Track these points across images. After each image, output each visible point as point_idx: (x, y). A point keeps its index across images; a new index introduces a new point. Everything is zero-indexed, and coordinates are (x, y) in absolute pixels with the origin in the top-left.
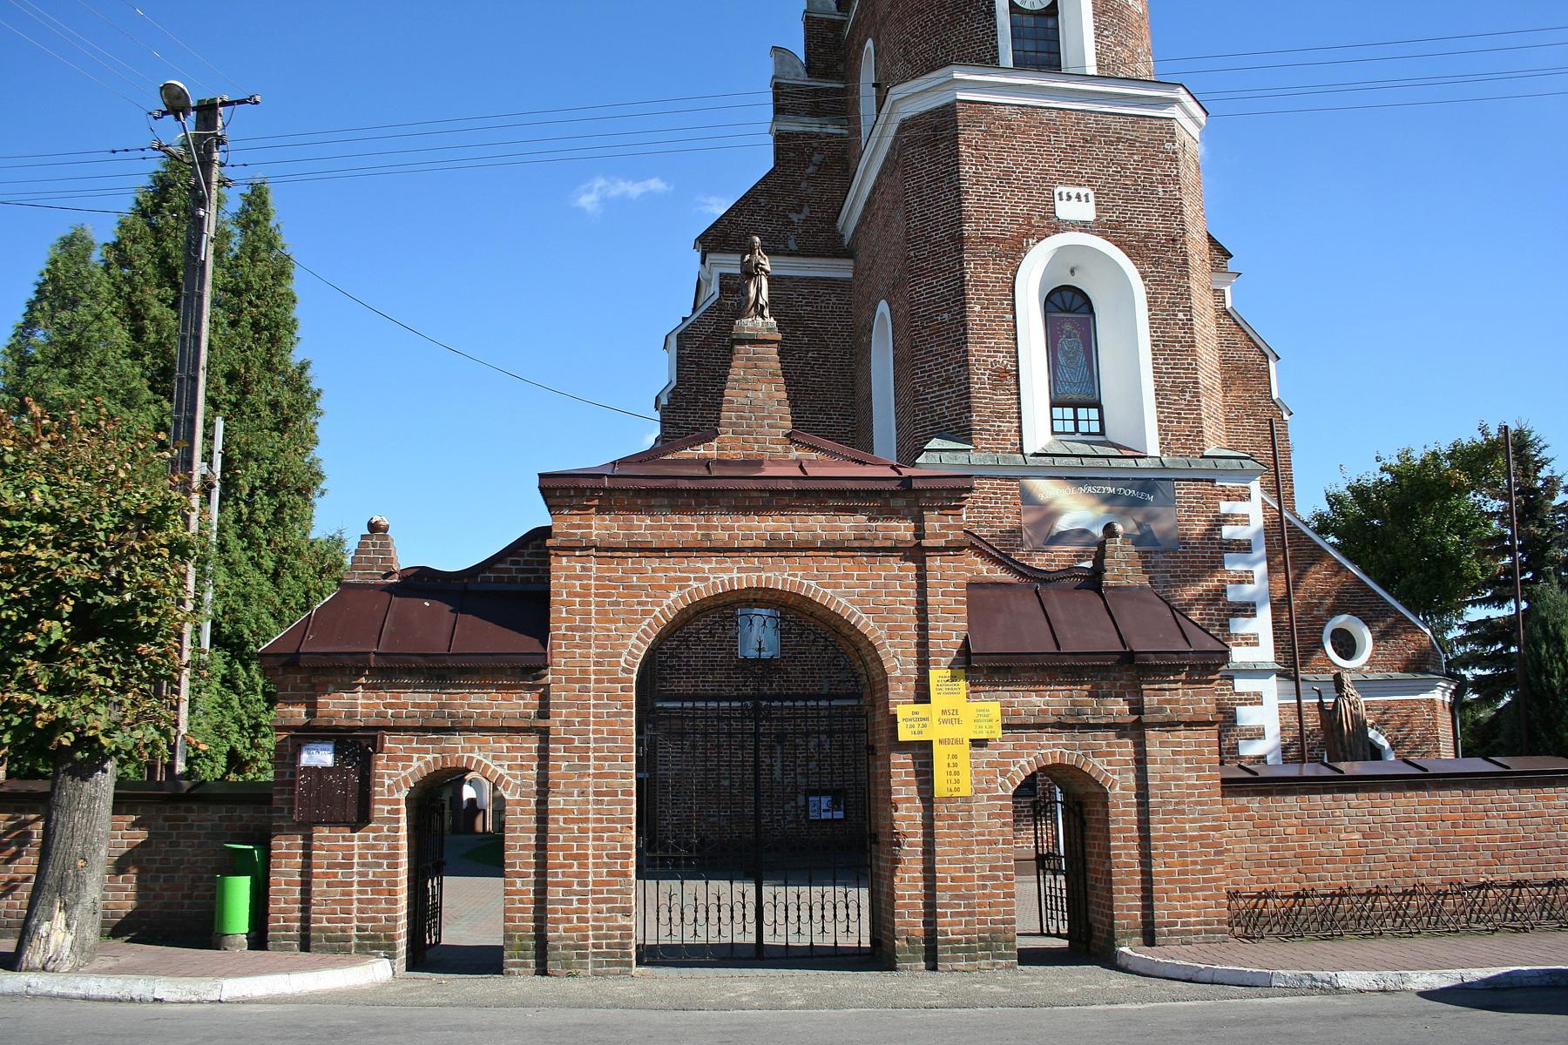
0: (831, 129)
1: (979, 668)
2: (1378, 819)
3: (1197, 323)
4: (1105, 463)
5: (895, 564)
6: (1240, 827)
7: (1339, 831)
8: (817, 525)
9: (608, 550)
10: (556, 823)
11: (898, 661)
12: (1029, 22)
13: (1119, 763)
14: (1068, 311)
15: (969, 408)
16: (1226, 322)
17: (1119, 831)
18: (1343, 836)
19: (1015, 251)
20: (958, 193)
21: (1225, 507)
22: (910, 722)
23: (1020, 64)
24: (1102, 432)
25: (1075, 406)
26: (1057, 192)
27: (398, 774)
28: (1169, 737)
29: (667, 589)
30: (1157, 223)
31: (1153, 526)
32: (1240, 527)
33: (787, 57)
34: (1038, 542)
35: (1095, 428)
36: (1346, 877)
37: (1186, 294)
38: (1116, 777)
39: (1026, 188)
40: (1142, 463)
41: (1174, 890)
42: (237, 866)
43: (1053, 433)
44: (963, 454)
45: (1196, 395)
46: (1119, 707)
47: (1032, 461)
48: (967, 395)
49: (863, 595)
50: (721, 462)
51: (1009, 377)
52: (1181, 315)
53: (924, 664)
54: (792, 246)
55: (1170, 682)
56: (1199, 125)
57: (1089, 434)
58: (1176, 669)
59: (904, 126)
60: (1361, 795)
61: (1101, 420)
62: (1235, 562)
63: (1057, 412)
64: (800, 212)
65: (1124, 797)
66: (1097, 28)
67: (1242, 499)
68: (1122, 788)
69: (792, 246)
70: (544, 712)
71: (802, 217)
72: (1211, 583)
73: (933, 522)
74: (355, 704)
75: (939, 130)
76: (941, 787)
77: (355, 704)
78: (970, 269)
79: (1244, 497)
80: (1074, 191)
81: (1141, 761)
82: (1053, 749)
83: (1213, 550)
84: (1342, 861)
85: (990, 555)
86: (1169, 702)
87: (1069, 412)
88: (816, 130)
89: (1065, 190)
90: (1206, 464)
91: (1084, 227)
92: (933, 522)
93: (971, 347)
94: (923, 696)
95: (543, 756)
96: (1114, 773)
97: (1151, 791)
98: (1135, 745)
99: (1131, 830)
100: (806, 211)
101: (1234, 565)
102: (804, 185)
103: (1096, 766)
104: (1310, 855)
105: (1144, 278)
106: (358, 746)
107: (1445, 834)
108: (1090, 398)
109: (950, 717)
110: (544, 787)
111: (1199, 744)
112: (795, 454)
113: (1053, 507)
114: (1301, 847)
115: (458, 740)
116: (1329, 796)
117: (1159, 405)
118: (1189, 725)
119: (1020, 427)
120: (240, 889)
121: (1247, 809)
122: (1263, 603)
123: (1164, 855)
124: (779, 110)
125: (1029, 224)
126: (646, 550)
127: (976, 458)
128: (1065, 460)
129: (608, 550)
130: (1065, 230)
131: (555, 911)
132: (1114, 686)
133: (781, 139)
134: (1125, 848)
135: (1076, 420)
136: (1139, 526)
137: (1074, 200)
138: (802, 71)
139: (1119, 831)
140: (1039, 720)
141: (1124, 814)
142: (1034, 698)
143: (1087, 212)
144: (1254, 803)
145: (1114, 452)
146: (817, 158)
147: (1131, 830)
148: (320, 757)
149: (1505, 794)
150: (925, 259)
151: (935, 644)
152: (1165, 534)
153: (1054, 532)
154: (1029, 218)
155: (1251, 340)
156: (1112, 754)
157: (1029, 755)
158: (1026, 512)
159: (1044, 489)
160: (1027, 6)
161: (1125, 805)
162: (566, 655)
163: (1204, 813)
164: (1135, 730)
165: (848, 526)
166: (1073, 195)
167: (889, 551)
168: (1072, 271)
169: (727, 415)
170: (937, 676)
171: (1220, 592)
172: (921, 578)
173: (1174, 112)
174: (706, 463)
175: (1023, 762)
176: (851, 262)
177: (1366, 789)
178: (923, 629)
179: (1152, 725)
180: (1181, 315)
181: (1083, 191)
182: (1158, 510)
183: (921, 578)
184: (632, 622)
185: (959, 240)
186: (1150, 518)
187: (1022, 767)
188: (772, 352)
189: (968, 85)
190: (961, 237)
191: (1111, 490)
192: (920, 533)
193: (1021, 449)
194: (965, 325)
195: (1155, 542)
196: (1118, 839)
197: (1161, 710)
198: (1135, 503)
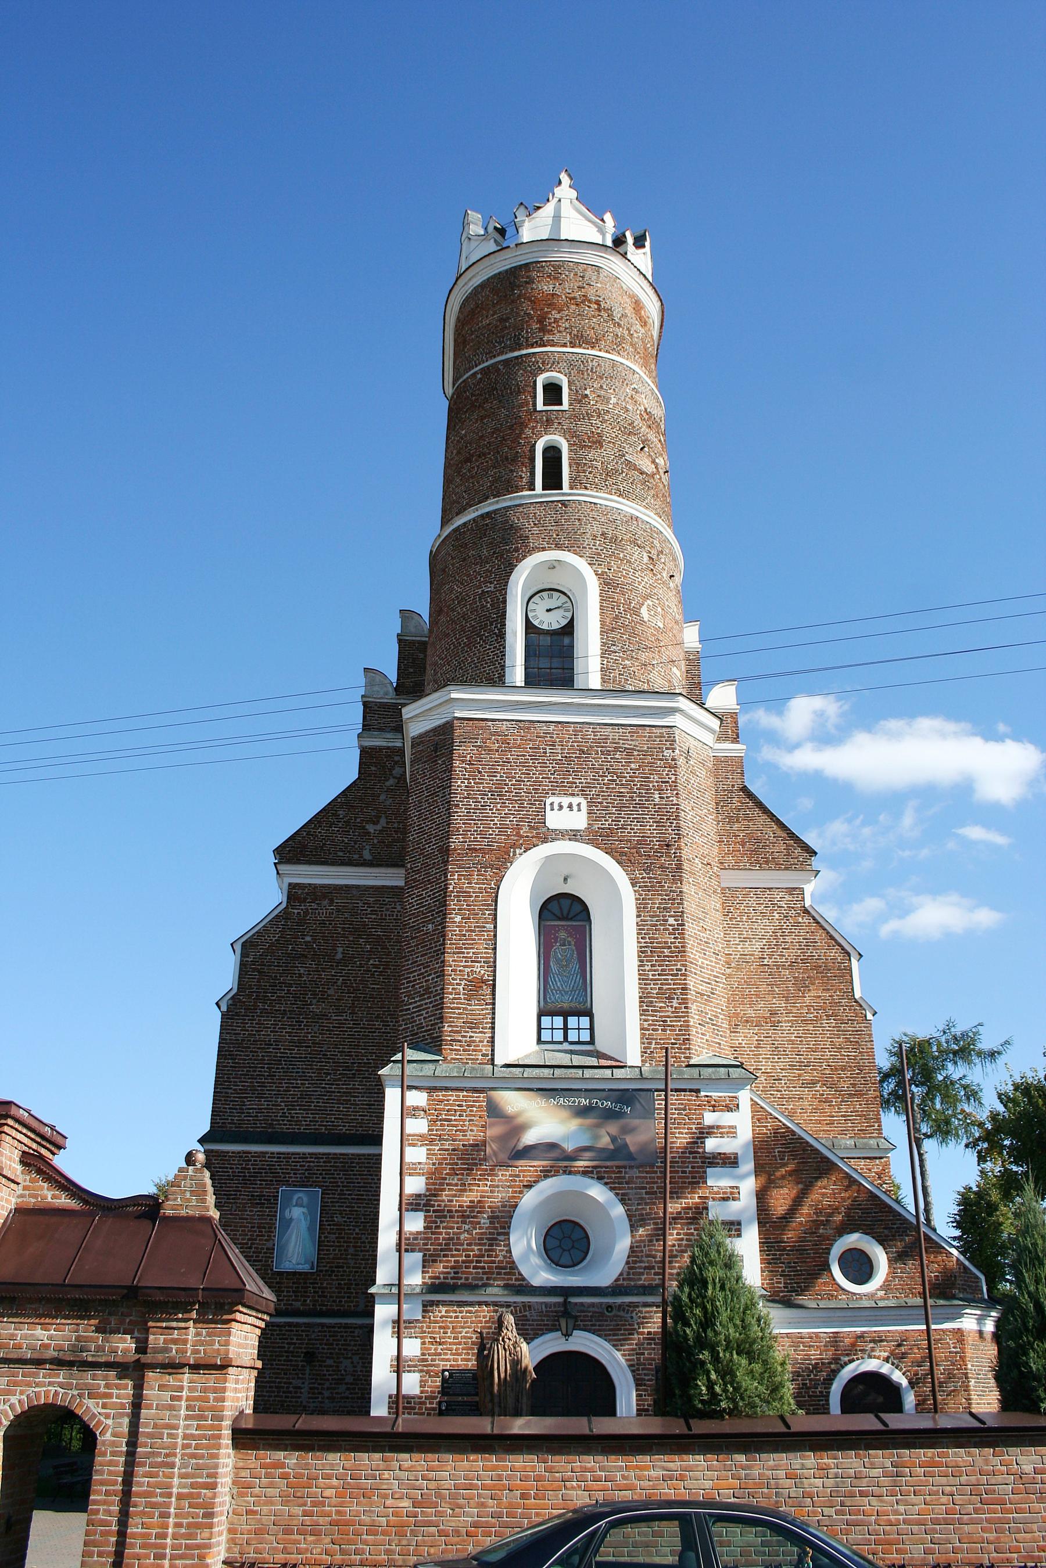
2: (433, 1485)
6: (271, 1486)
7: (386, 1497)
12: (547, 640)
13: (114, 1406)
14: (566, 919)
15: (441, 1018)
16: (804, 920)
17: (103, 1483)
18: (389, 1502)
19: (501, 862)
21: (710, 1118)
23: (532, 681)
24: (592, 1042)
25: (566, 1014)
26: (548, 801)
28: (171, 1380)
31: (629, 1139)
32: (726, 1140)
33: (378, 678)
34: (503, 1156)
35: (585, 1036)
36: (388, 1552)
38: (110, 1422)
40: (619, 1073)
41: (148, 1557)
43: (539, 1041)
44: (432, 1066)
45: (684, 1002)
46: (125, 1345)
47: (499, 1072)
48: (440, 1006)
51: (485, 987)
52: (671, 921)
54: (367, 855)
55: (178, 1320)
56: (712, 731)
57: (579, 1043)
58: (186, 1308)
60: (416, 1456)
61: (592, 1029)
62: (719, 1177)
63: (546, 1021)
64: (375, 823)
65: (113, 1444)
66: (604, 644)
67: (729, 1109)
68: (114, 1435)
69: (367, 855)
71: (379, 827)
72: (692, 1199)
78: (454, 880)
79: (732, 1107)
80: (566, 801)
81: (137, 1405)
82: (49, 1388)
83: (697, 1163)
84: (384, 1533)
85: (56, 1181)
86: (175, 1341)
87: (559, 1021)
89: (556, 800)
90: (688, 1073)
91: (574, 835)
93: (448, 958)
96: (107, 1416)
97: (142, 1439)
98: (135, 1387)
99: (115, 1483)
100: (383, 822)
101: (717, 1180)
102: (382, 797)
103: (90, 1408)
104: (347, 1524)
105: (633, 885)
107: (511, 1506)
108: (581, 1007)
111: (205, 1390)
113: (520, 1120)
114: (338, 1512)
116: (378, 1456)
117: (643, 1012)
118: (195, 1368)
119: (493, 1037)
121: (283, 1466)
122: (750, 1222)
123: (143, 1514)
124: (367, 727)
125: (518, 835)
127: (442, 1069)
130: (553, 840)
132: (122, 1322)
133: (366, 754)
134: (105, 1502)
135: (566, 1029)
136: (614, 1139)
137: (565, 810)
138: (391, 690)
139: (103, 1483)
140: (36, 1356)
141: (111, 1463)
142: (39, 1332)
143: (579, 820)
144: (291, 1459)
147: (115, 1483)
149: (590, 1461)
150: (419, 872)
152: (643, 1148)
153: (521, 1146)
154: (518, 828)
155: (832, 938)
156: (109, 1396)
157: (22, 1393)
158: (492, 1125)
159: (513, 1101)
160: (545, 627)
161: (114, 1454)
163: (198, 1468)
164: (134, 1371)
166: (565, 805)
168: (565, 879)
171: (699, 1211)
173: (677, 720)
175: (14, 1400)
176: (402, 871)
177: (422, 1449)
179: (152, 1367)
180: (671, 921)
181: (575, 801)
182: (636, 1122)
185: (445, 851)
186: (626, 1130)
190: (448, 850)
191: (584, 1102)
193: (493, 1059)
195: (630, 1157)
196: (99, 1493)
197: (167, 1350)
198: (610, 1115)
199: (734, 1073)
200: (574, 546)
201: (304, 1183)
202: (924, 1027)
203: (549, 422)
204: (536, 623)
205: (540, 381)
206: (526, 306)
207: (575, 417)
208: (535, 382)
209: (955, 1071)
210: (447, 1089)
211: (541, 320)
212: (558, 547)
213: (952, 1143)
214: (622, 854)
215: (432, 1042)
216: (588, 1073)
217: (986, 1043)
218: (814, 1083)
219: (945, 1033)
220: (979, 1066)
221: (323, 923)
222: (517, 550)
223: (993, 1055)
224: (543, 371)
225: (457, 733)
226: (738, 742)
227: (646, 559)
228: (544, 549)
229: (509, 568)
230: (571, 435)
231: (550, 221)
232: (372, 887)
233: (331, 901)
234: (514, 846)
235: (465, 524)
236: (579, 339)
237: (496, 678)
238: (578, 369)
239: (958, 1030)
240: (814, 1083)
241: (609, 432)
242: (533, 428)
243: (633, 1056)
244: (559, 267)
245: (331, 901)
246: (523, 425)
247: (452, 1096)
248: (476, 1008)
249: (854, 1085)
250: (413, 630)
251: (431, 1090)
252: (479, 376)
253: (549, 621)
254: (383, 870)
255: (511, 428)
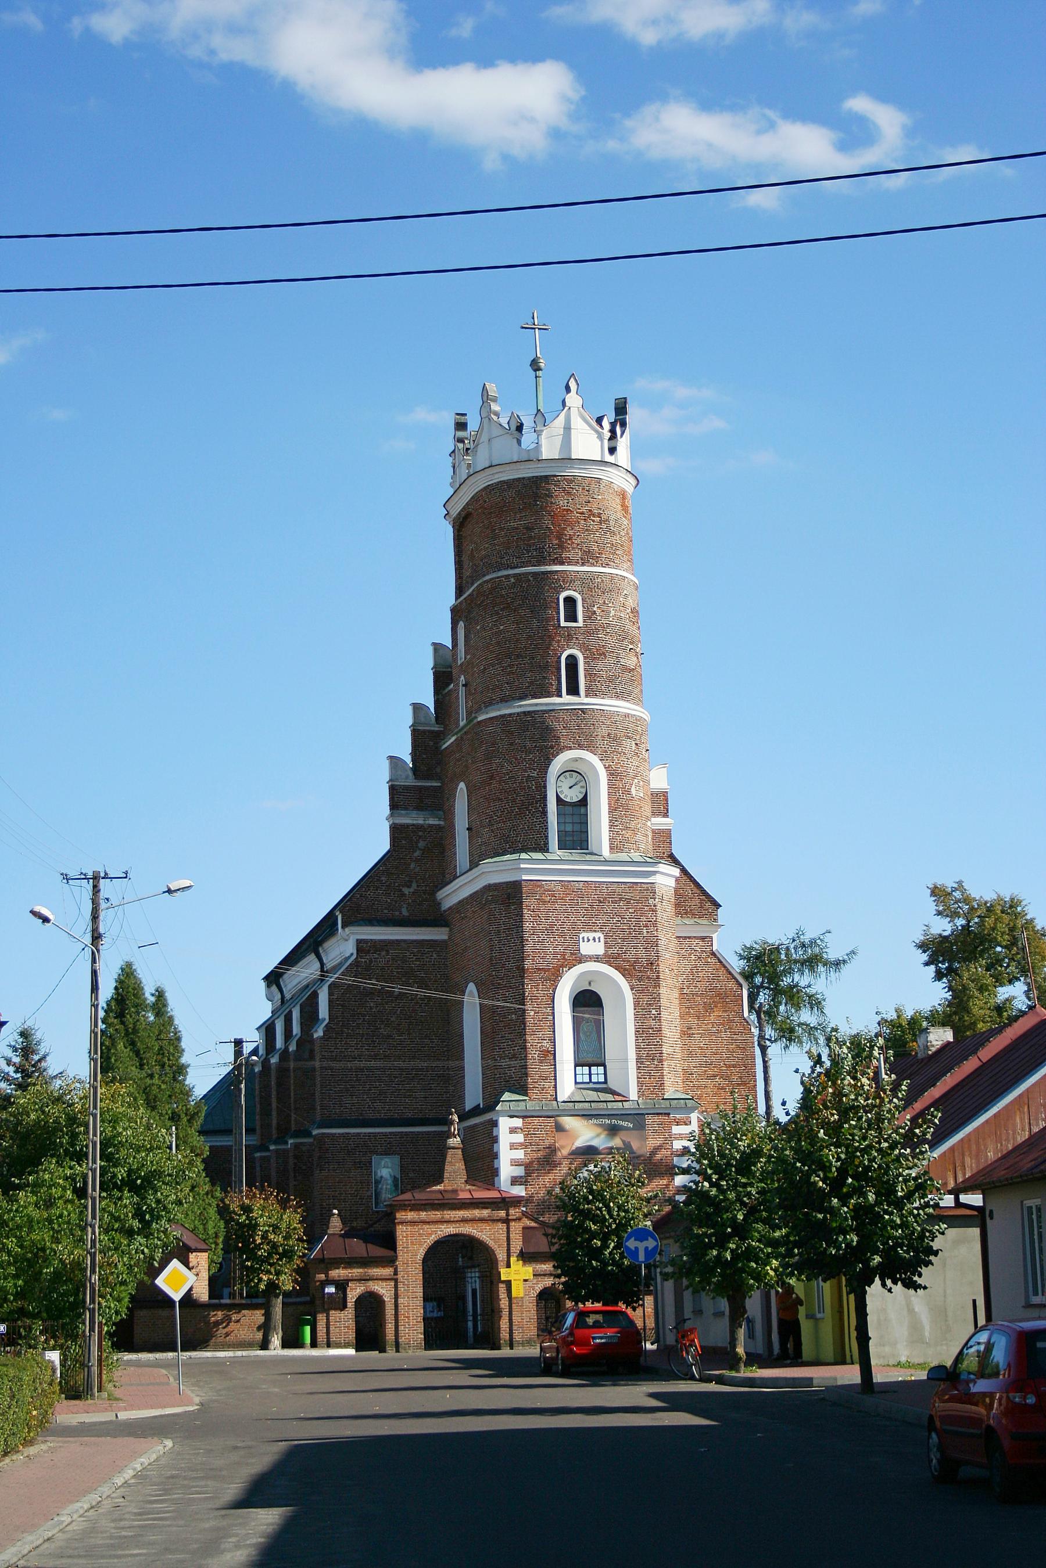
0: (432, 821)
1: (526, 1257)
3: (664, 1015)
4: (603, 1105)
5: (500, 1225)
8: (477, 1213)
9: (413, 1223)
10: (401, 1307)
11: (501, 1255)
15: (526, 1075)
16: (713, 960)
19: (555, 976)
20: (522, 940)
22: (505, 1274)
24: (606, 1082)
25: (590, 1066)
27: (354, 1292)
29: (431, 1234)
30: (642, 953)
35: (602, 1079)
37: (657, 998)
39: (562, 935)
40: (626, 1105)
42: (307, 1322)
44: (523, 1103)
47: (562, 1106)
49: (489, 1234)
50: (445, 1191)
51: (550, 1055)
52: (654, 1012)
53: (509, 1256)
59: (488, 888)
61: (605, 1074)
64: (409, 887)
66: (610, 821)
70: (396, 1273)
71: (412, 890)
73: (512, 1211)
74: (337, 1273)
75: (510, 895)
76: (514, 1294)
77: (337, 1273)
80: (591, 935)
87: (586, 1069)
88: (421, 822)
91: (597, 959)
92: (512, 1211)
93: (528, 1038)
94: (508, 1266)
95: (396, 1287)
100: (414, 885)
102: (412, 866)
105: (632, 989)
106: (342, 1286)
108: (599, 1061)
109: (517, 1272)
110: (396, 1297)
112: (468, 1187)
115: (371, 1283)
117: (638, 1068)
120: (307, 1329)
124: (394, 806)
125: (564, 958)
126: (424, 1222)
128: (581, 1104)
129: (413, 1223)
131: (401, 1333)
133: (396, 831)
135: (590, 1075)
137: (591, 941)
138: (410, 773)
143: (599, 949)
145: (610, 1097)
146: (421, 844)
148: (331, 1290)
151: (512, 1249)
160: (568, 800)
162: (402, 1256)
165: (486, 1213)
167: (498, 1220)
169: (446, 1175)
170: (513, 1259)
172: (508, 1228)
174: (440, 1192)
178: (509, 1244)
180: (654, 1012)
181: (597, 935)
183: (508, 1228)
184: (421, 1245)
185: (522, 970)
187: (539, 1287)
188: (460, 1152)
189: (528, 868)
190: (523, 969)
192: (508, 1215)
194: (524, 1024)
199: (685, 1106)
200: (591, 748)
201: (386, 1153)
202: (778, 934)
203: (569, 637)
204: (562, 796)
205: (563, 595)
206: (547, 522)
207: (589, 632)
208: (558, 599)
209: (802, 979)
210: (533, 1117)
211: (560, 536)
212: (581, 747)
213: (794, 1048)
214: (625, 970)
215: (522, 1089)
216: (610, 1105)
217: (832, 955)
218: (715, 1076)
219: (794, 941)
220: (823, 976)
221: (383, 968)
222: (552, 747)
223: (838, 964)
224: (564, 589)
225: (524, 890)
226: (667, 816)
227: (634, 745)
228: (570, 748)
229: (548, 762)
230: (584, 648)
231: (562, 431)
232: (415, 941)
233: (387, 951)
234: (562, 966)
235: (510, 715)
236: (589, 557)
237: (544, 848)
238: (589, 585)
239: (806, 939)
240: (715, 1076)
241: (611, 641)
242: (559, 641)
243: (633, 1095)
244: (572, 481)
245: (387, 951)
246: (551, 638)
247: (536, 1120)
248: (546, 1067)
249: (741, 1078)
250: (423, 720)
251: (524, 1117)
252: (512, 580)
253: (572, 796)
254: (423, 929)
255: (542, 638)
